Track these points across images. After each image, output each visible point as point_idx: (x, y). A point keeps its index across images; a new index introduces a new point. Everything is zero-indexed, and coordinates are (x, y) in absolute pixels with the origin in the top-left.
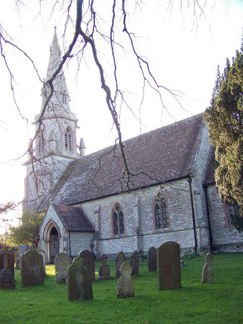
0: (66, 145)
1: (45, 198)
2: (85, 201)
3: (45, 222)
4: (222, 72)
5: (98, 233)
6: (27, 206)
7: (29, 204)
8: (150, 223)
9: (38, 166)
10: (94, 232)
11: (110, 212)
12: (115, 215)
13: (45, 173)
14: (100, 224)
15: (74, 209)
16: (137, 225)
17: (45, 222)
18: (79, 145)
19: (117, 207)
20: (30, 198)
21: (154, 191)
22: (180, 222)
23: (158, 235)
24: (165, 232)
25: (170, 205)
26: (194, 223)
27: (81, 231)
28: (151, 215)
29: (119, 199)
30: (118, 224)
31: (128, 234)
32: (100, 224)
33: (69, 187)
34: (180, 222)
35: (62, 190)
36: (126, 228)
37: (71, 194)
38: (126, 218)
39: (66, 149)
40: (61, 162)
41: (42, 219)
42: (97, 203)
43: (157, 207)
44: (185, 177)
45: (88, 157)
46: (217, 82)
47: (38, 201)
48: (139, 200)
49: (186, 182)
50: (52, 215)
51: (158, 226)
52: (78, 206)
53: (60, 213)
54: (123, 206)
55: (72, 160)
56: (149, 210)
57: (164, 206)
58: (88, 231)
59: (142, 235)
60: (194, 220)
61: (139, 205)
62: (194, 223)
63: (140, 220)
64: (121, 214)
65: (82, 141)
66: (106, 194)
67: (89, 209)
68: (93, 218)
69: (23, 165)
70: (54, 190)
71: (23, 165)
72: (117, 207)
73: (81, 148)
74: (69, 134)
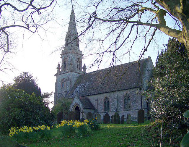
0: (78, 67)
1: (67, 93)
2: (90, 95)
3: (73, 103)
4: (160, 54)
5: (97, 110)
6: (56, 96)
7: (57, 95)
8: (122, 106)
9: (64, 76)
10: (95, 109)
11: (103, 101)
12: (105, 102)
13: (68, 80)
14: (98, 106)
15: (86, 98)
16: (116, 107)
17: (73, 103)
18: (83, 67)
19: (107, 98)
20: (58, 92)
21: (124, 93)
22: (136, 106)
23: (125, 111)
24: (129, 110)
25: (131, 99)
26: (142, 107)
27: (89, 109)
28: (123, 103)
29: (108, 95)
30: (107, 106)
31: (112, 111)
32: (98, 106)
33: (80, 88)
34: (136, 106)
35: (77, 89)
36: (111, 108)
37: (82, 92)
38: (111, 104)
39: (78, 69)
40: (73, 76)
41: (71, 103)
42: (96, 96)
43: (125, 99)
44: (139, 87)
45: (89, 74)
46: (158, 57)
47: (64, 94)
48: (117, 96)
49: (139, 89)
50: (77, 101)
51: (125, 107)
52: (87, 97)
53: (80, 100)
54: (109, 98)
55: (80, 75)
56: (122, 100)
57: (129, 99)
58: (92, 109)
59: (118, 111)
60: (142, 105)
61: (117, 98)
62: (142, 107)
63: (117, 104)
64: (108, 101)
65: (85, 64)
66: (101, 92)
67: (92, 99)
68: (94, 103)
69: (54, 75)
70: (72, 89)
71: (54, 75)
72: (107, 98)
73: (85, 68)
74: (79, 61)
